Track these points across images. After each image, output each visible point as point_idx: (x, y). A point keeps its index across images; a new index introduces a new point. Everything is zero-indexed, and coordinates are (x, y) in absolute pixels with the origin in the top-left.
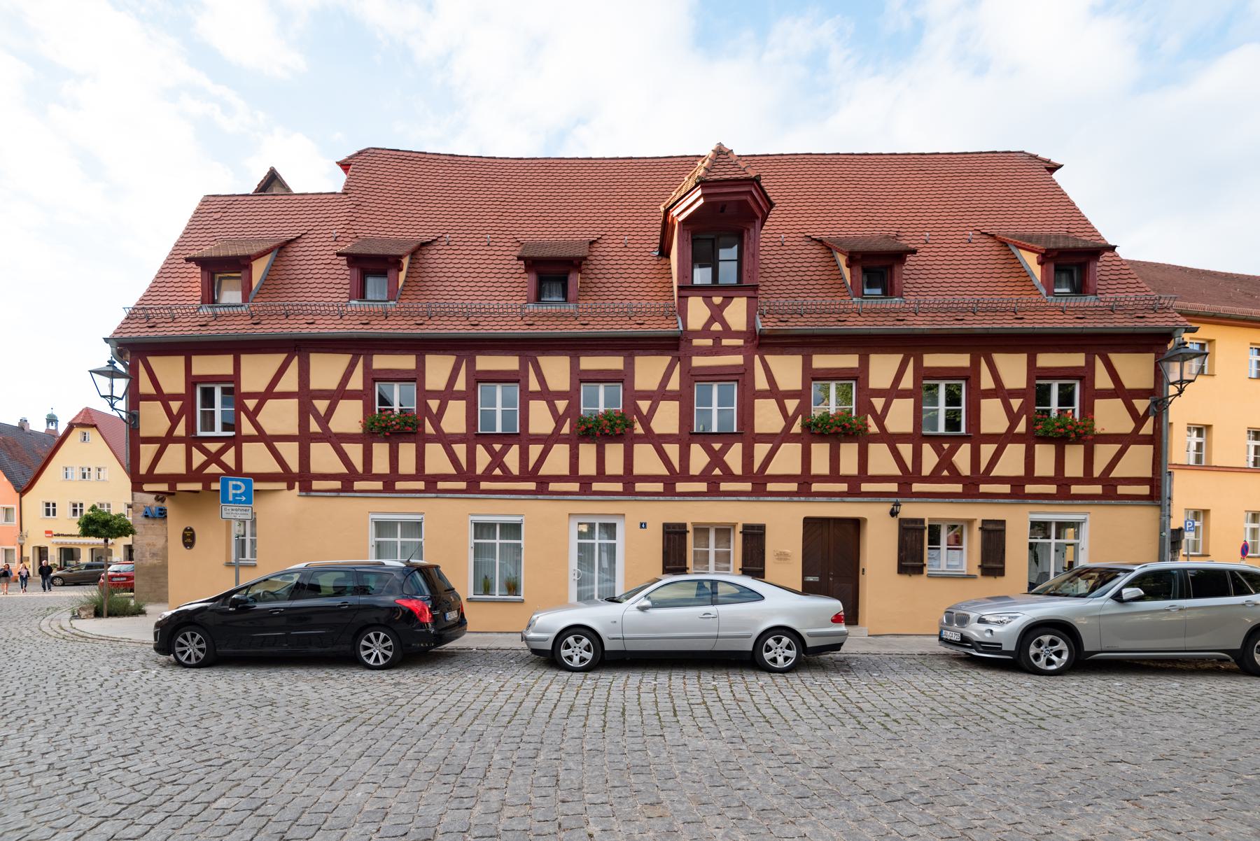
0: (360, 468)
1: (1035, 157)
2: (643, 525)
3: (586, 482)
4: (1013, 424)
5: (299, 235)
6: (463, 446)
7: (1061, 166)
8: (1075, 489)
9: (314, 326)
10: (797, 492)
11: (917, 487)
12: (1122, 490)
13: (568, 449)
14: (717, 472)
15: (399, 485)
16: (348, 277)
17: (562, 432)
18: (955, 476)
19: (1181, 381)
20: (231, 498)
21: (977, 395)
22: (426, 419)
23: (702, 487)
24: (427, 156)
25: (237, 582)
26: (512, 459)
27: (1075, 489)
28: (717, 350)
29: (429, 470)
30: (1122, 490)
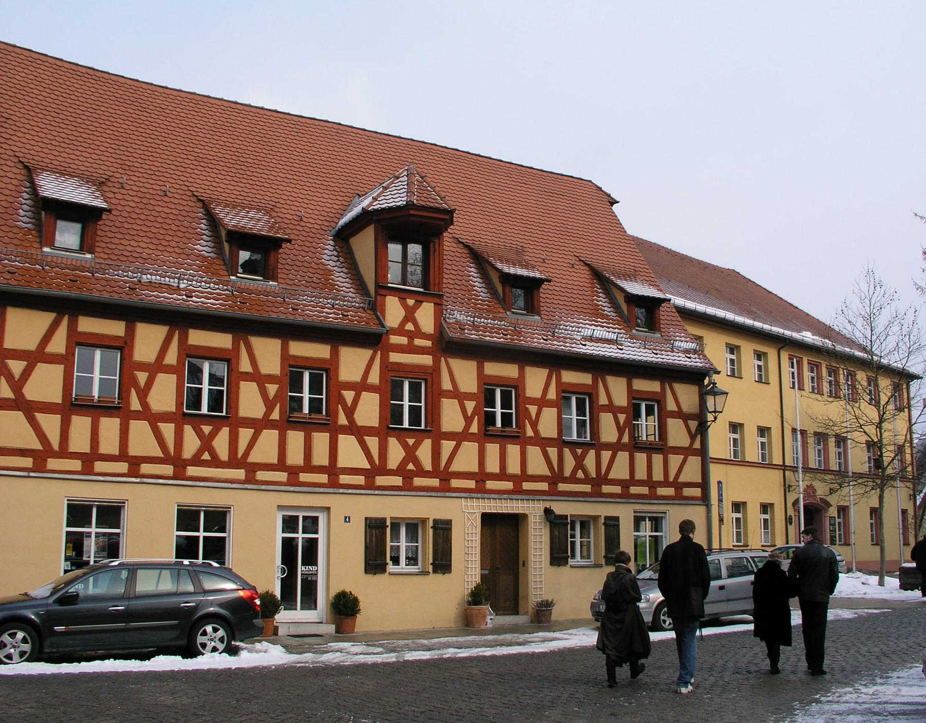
0: (56, 446)
1: (600, 189)
2: (347, 519)
3: (293, 472)
4: (269, 410)
7: (618, 202)
10: (512, 491)
11: (562, 487)
13: (90, 423)
14: (411, 466)
15: (99, 466)
18: (587, 480)
19: (715, 412)
21: (236, 377)
22: (278, 404)
25: (160, 573)
26: (221, 443)
28: (410, 349)
29: (133, 451)
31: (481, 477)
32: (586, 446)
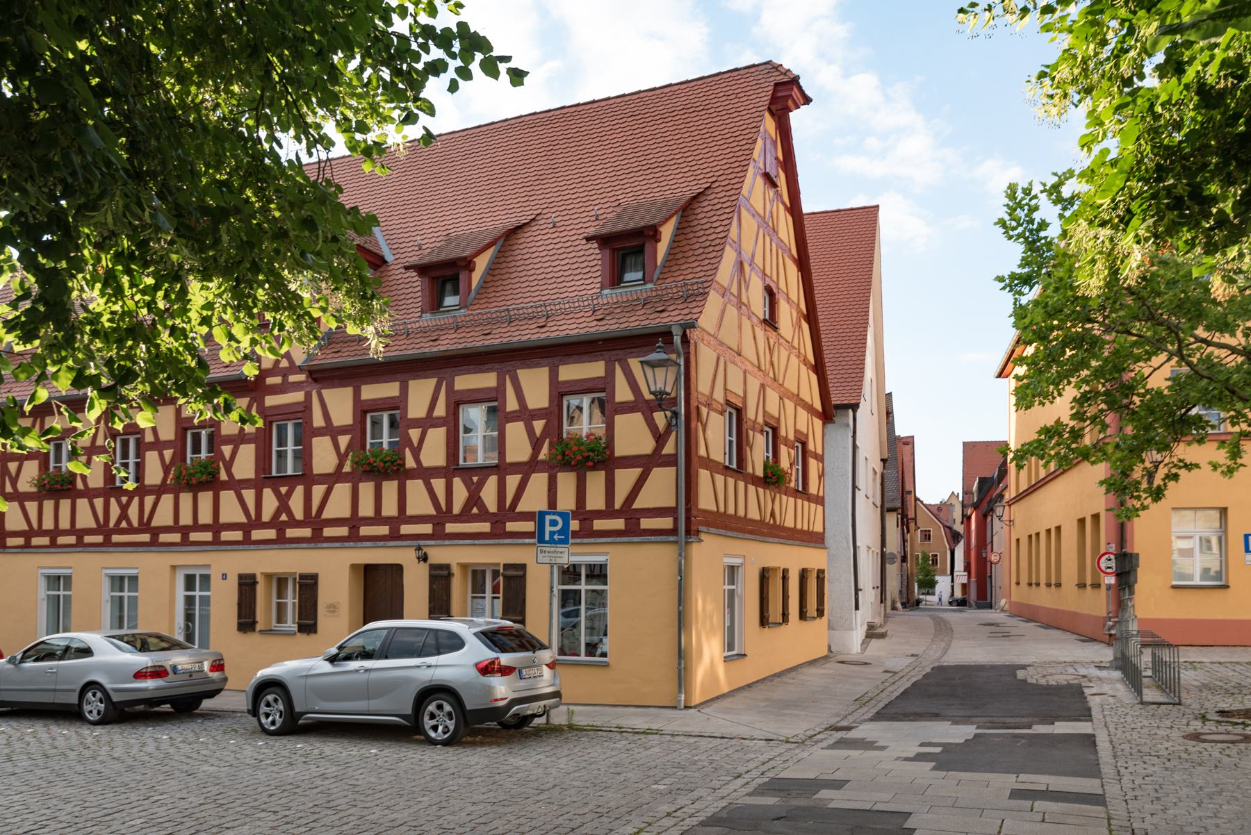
3: (185, 531)
5: (533, 217)
6: (35, 504)
8: (599, 525)
9: (665, 314)
10: (432, 535)
11: (451, 528)
12: (646, 523)
16: (600, 262)
17: (344, 471)
18: (484, 515)
20: (547, 538)
23: (271, 534)
24: (497, 126)
27: (599, 525)
29: (79, 525)
30: (646, 523)
31: (354, 522)
32: (292, 481)
